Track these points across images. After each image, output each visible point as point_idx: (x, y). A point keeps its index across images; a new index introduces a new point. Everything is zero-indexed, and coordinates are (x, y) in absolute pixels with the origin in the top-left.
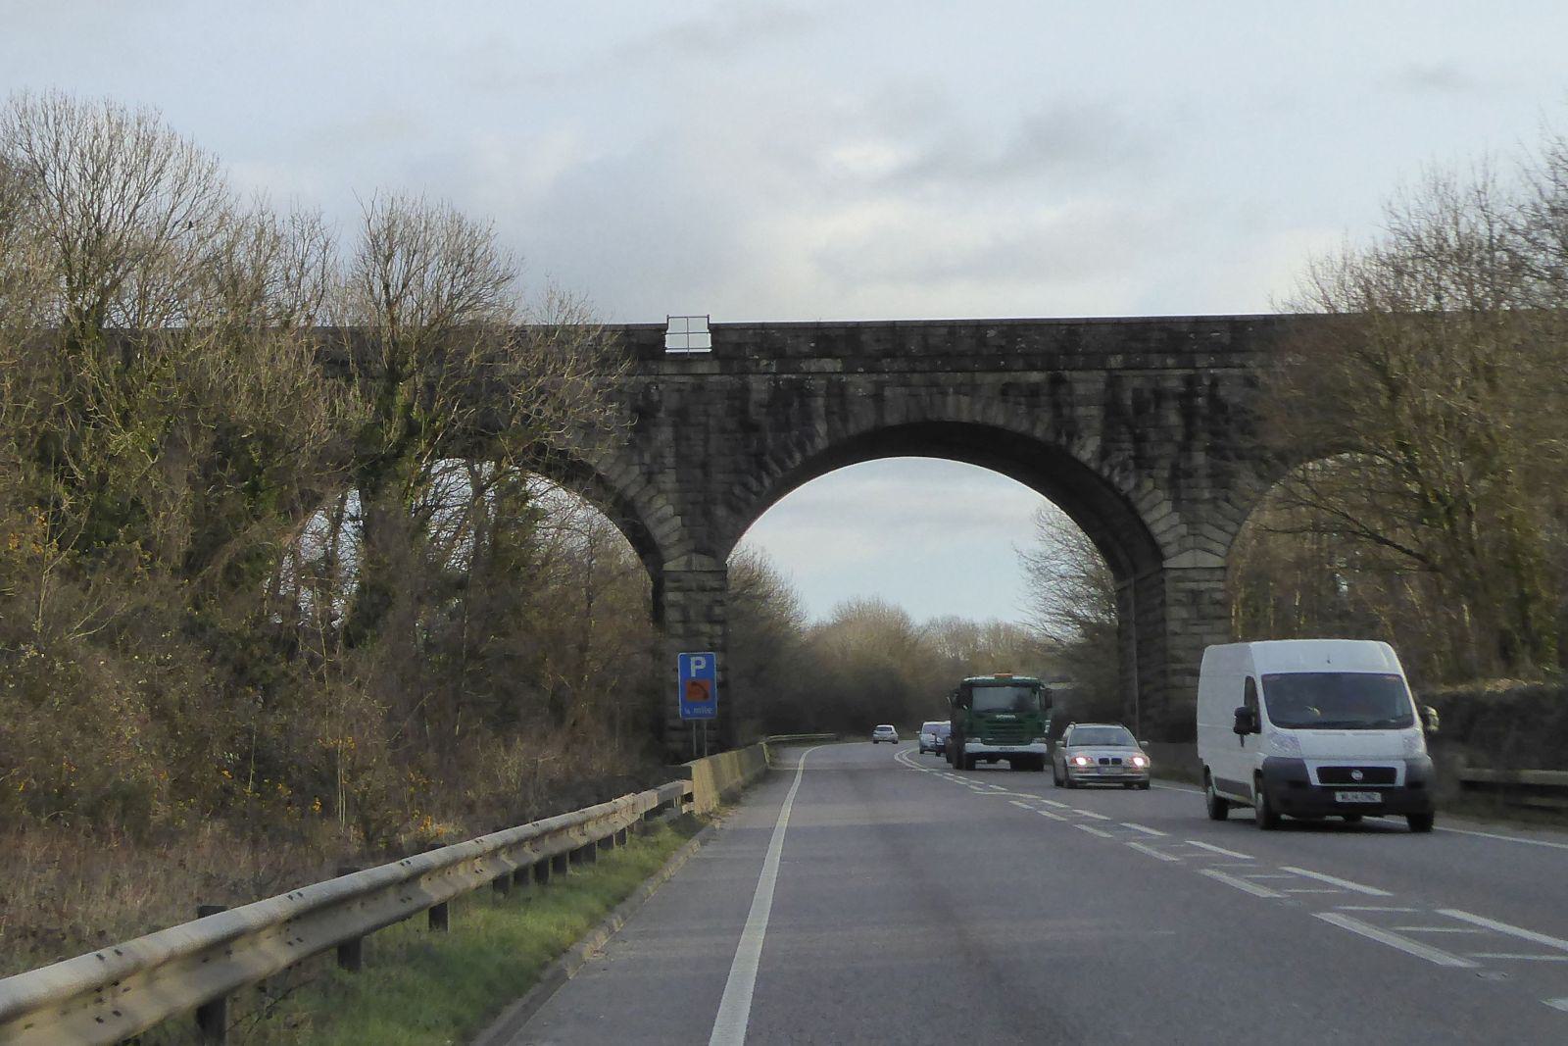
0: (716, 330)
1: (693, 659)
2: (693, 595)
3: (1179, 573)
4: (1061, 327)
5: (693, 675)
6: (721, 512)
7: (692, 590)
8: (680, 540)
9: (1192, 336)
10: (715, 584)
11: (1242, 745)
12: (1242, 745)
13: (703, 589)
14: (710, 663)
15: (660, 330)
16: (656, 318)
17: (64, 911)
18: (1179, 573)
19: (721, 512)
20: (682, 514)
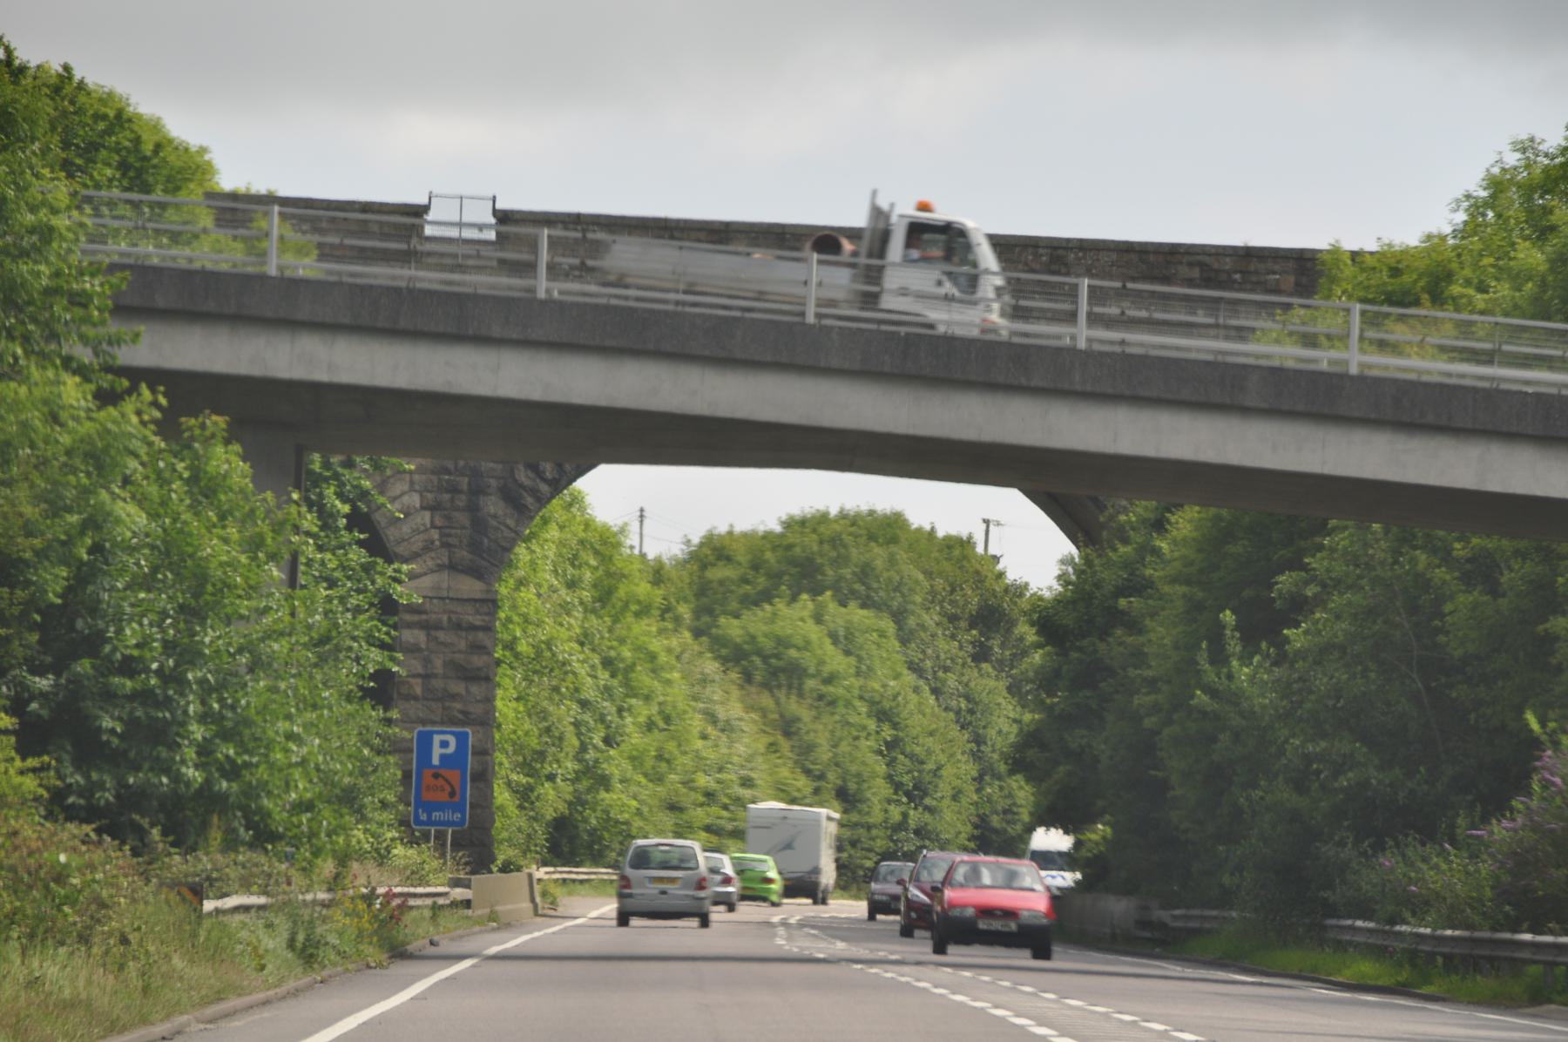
0: (503, 217)
1: (437, 739)
2: (441, 635)
3: (667, 848)
4: (1041, 251)
5: (436, 761)
6: (493, 506)
7: (442, 628)
8: (428, 547)
9: (1237, 276)
10: (477, 620)
11: (642, 510)
12: (642, 510)
13: (458, 627)
14: (462, 739)
15: (419, 211)
16: (414, 196)
17: (209, 905)
18: (667, 848)
19: (493, 506)
20: (433, 508)
